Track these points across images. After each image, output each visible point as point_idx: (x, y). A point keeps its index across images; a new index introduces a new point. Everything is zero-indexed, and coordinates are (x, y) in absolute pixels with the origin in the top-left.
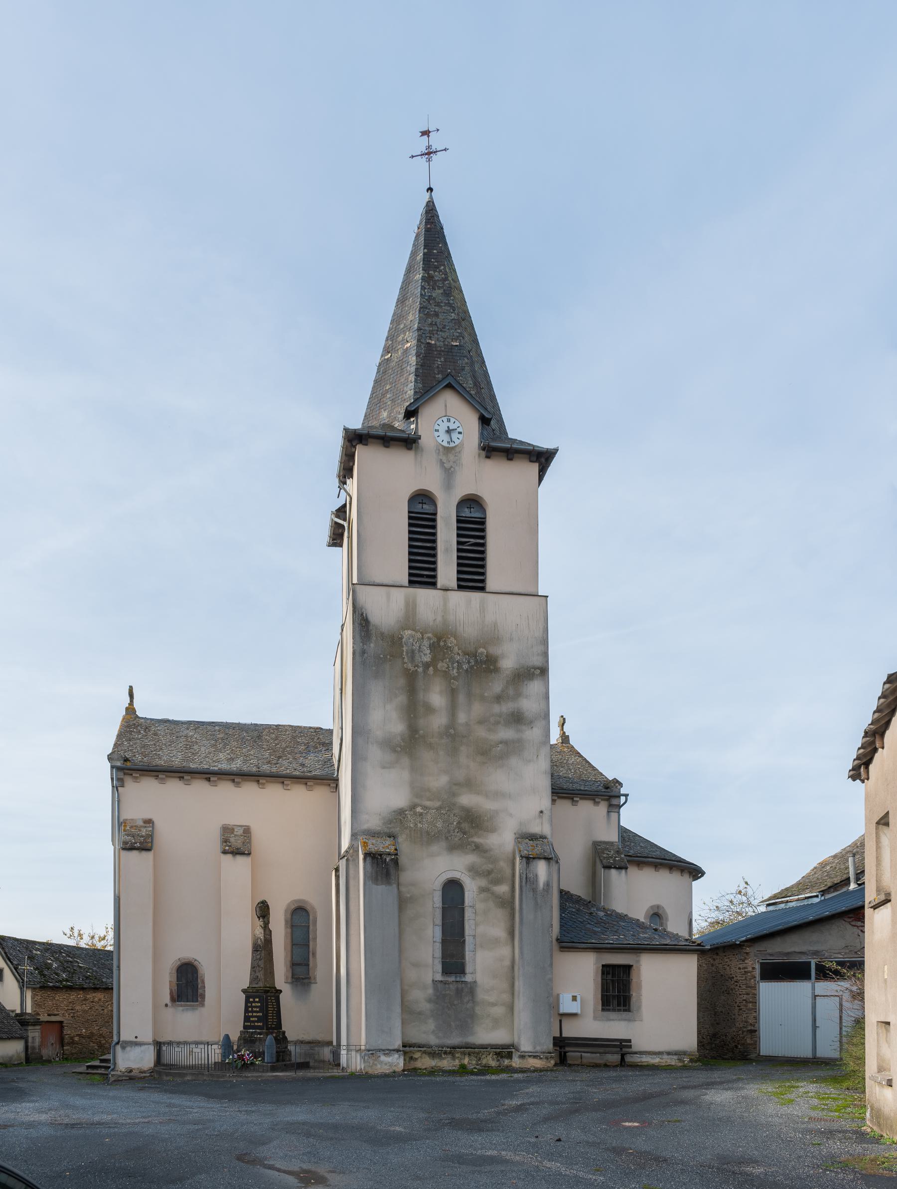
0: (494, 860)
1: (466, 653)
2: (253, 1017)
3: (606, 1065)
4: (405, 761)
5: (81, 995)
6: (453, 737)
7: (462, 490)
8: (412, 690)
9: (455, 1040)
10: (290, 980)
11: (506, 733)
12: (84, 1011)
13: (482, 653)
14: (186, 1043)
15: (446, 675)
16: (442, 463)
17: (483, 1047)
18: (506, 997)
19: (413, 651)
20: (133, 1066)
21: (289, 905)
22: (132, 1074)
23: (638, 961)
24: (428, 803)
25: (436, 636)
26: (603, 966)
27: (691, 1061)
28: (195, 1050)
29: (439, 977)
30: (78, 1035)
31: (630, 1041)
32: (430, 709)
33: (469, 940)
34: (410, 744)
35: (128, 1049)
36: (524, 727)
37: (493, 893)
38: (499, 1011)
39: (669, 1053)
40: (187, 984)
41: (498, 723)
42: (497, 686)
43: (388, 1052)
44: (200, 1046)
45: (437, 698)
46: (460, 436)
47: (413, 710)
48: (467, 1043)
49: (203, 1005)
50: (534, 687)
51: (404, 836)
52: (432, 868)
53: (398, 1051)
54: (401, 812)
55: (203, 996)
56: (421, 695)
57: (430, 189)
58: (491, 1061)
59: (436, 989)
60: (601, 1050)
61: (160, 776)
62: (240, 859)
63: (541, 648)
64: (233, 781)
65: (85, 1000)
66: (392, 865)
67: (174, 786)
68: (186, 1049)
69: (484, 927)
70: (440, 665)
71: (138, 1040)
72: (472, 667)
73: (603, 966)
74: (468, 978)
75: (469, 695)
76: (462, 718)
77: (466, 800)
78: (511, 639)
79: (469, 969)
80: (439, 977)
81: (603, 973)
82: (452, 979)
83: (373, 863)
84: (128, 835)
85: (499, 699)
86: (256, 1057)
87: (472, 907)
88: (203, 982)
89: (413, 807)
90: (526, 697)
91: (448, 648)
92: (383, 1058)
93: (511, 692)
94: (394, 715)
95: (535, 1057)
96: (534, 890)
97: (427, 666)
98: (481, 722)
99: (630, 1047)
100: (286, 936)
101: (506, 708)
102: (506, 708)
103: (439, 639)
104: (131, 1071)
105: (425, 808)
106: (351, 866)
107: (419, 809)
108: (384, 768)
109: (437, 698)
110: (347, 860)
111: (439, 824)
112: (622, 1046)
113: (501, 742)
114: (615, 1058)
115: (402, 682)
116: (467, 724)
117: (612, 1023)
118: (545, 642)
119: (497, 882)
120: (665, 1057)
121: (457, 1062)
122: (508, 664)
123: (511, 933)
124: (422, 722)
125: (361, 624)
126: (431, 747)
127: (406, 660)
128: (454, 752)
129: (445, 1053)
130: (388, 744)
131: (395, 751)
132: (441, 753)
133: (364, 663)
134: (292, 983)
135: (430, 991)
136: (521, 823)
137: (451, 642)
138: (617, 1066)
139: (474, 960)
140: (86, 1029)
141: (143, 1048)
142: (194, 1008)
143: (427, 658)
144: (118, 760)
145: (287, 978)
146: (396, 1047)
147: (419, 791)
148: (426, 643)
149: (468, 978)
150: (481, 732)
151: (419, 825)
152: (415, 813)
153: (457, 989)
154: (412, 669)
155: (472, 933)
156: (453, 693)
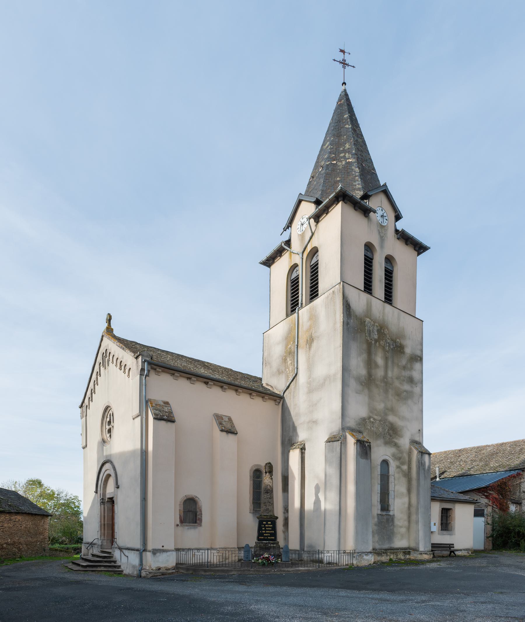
0: (401, 452)
1: (392, 340)
2: (266, 533)
3: (443, 557)
4: (366, 391)
5: (8, 517)
6: (386, 382)
7: (388, 251)
8: (369, 353)
9: (386, 546)
10: (252, 511)
11: (406, 387)
12: (9, 527)
13: (398, 342)
14: (189, 549)
15: (384, 348)
16: (379, 233)
17: (397, 549)
18: (406, 523)
19: (370, 331)
20: (162, 565)
21: (252, 467)
22: (161, 571)
23: (454, 507)
24: (376, 417)
25: (380, 325)
26: (442, 509)
27: (472, 553)
28: (196, 553)
29: (379, 512)
30: (5, 543)
31: (453, 544)
32: (377, 366)
33: (391, 493)
34: (368, 382)
35: (158, 554)
36: (414, 386)
37: (401, 469)
38: (403, 530)
39: (464, 550)
40: (190, 513)
41: (404, 381)
42: (404, 362)
43: (367, 553)
44: (201, 551)
45: (380, 360)
46: (387, 222)
47: (370, 364)
48: (391, 547)
49: (201, 525)
50: (417, 366)
51: (366, 433)
52: (380, 452)
53: (371, 553)
54: (364, 420)
55: (201, 520)
56: (373, 356)
57: (344, 83)
58: (401, 556)
59: (378, 518)
60: (440, 549)
61: (176, 374)
62: (231, 436)
63: (419, 347)
64: (222, 387)
65: (10, 520)
66: (368, 448)
67: (183, 383)
68: (190, 553)
69: (398, 486)
70: (381, 342)
71: (164, 548)
72: (394, 348)
73: (442, 509)
74: (391, 513)
75: (393, 362)
76: (390, 374)
77: (391, 418)
78: (409, 339)
79: (391, 508)
80: (379, 512)
81: (442, 513)
82: (384, 513)
83: (360, 446)
84: (156, 410)
85: (404, 368)
86: (278, 559)
87: (393, 475)
88: (201, 511)
89: (369, 418)
90: (415, 370)
91: (385, 334)
92: (365, 557)
93: (409, 366)
94: (362, 364)
95: (426, 554)
96: (424, 469)
97: (376, 341)
98: (398, 378)
99: (453, 547)
100: (250, 485)
101: (406, 373)
102: (406, 373)
103: (381, 328)
104: (160, 569)
105: (374, 419)
106: (342, 446)
107: (372, 420)
108: (357, 393)
109: (380, 360)
110: (341, 443)
111: (381, 429)
112: (449, 547)
113: (405, 391)
114: (447, 553)
115: (365, 346)
116: (392, 378)
117: (444, 536)
118: (422, 344)
119: (403, 463)
120: (463, 551)
121: (388, 558)
122: (408, 351)
123: (409, 491)
124: (373, 371)
125: (346, 307)
126: (377, 386)
127: (367, 335)
128: (386, 391)
129: (384, 553)
130: (358, 379)
131: (362, 385)
132: (381, 391)
133: (348, 329)
134: (253, 513)
135: (376, 520)
136: (412, 435)
137: (386, 331)
138: (447, 557)
139: (394, 504)
140: (11, 539)
141: (169, 553)
142: (195, 527)
143: (376, 337)
144: (147, 356)
145: (250, 510)
146: (370, 550)
147: (372, 410)
148: (376, 328)
149: (391, 513)
150: (397, 383)
151: (372, 428)
152: (370, 421)
153: (387, 519)
154: (370, 341)
155: (393, 489)
156: (386, 359)
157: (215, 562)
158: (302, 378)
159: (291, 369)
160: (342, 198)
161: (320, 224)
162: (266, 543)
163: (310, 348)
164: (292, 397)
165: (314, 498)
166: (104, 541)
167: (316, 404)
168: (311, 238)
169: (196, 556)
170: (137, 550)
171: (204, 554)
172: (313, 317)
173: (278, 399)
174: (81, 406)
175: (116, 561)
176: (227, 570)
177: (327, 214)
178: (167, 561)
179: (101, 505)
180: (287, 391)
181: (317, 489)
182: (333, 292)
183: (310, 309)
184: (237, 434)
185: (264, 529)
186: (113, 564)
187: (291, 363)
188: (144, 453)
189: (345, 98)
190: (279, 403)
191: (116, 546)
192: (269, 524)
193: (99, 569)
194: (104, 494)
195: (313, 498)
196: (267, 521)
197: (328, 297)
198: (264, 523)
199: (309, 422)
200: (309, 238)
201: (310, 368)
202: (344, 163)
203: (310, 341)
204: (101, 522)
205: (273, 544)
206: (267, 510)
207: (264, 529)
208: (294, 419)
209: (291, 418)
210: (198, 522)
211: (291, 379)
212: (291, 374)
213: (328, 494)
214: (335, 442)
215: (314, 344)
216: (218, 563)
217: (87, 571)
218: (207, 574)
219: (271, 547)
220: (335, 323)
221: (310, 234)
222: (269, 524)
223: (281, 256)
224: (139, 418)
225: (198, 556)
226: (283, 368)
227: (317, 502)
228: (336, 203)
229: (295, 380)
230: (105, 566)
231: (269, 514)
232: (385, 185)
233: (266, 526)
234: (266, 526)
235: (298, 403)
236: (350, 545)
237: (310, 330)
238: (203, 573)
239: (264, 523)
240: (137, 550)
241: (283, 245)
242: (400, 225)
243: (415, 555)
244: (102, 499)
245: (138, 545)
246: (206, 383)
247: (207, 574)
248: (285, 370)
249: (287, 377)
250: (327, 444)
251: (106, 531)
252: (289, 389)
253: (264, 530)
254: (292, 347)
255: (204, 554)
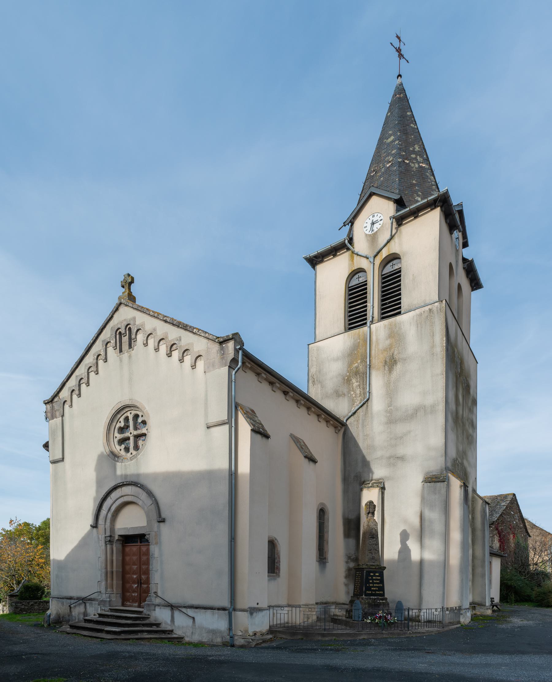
2: (373, 587)
49: (279, 576)
55: (278, 568)
57: (400, 76)
88: (279, 558)
157: (298, 622)
158: (377, 404)
159: (358, 392)
160: (441, 204)
161: (403, 228)
162: (375, 599)
163: (391, 370)
164: (360, 426)
165: (399, 546)
166: (112, 596)
167: (401, 438)
168: (388, 242)
169: (279, 615)
170: (224, 609)
171: (290, 612)
172: (396, 336)
173: (338, 424)
174: (50, 402)
175: (160, 624)
176: (355, 634)
177: (416, 218)
178: (260, 624)
179: (106, 544)
180: (352, 418)
181: (404, 536)
182: (430, 310)
183: (390, 324)
184: (316, 462)
185: (371, 581)
186: (154, 628)
187: (359, 386)
188: (233, 475)
189: (401, 90)
190: (339, 430)
191: (158, 601)
192: (377, 576)
193: (139, 636)
194: (112, 529)
195: (398, 546)
196: (374, 572)
197: (421, 315)
198: (372, 574)
199: (390, 458)
200: (385, 241)
201: (391, 393)
202: (417, 166)
203: (391, 363)
204: (106, 568)
205: (382, 600)
206: (373, 558)
207: (371, 581)
208: (365, 452)
209: (360, 450)
210: (276, 571)
211: (358, 404)
212: (359, 399)
213: (427, 541)
214: (439, 484)
215: (398, 367)
216: (302, 624)
217: (129, 639)
218: (327, 639)
219: (380, 604)
220: (433, 347)
221: (388, 237)
222: (377, 576)
223: (335, 255)
224: (227, 427)
225: (282, 615)
226: (345, 391)
227: (405, 551)
228: (433, 207)
229: (365, 406)
230: (108, 632)
231: (376, 564)
232: (461, 205)
233: (374, 578)
234: (374, 578)
235: (372, 434)
236: (454, 601)
237: (390, 349)
238: (320, 638)
239: (372, 574)
240: (224, 609)
241: (346, 241)
242: (467, 253)
243: (482, 610)
244: (110, 536)
245: (226, 603)
246: (285, 393)
247: (327, 639)
248: (349, 392)
249: (352, 402)
250: (426, 484)
251: (115, 582)
252: (356, 415)
253: (371, 583)
254: (361, 367)
255: (290, 612)
